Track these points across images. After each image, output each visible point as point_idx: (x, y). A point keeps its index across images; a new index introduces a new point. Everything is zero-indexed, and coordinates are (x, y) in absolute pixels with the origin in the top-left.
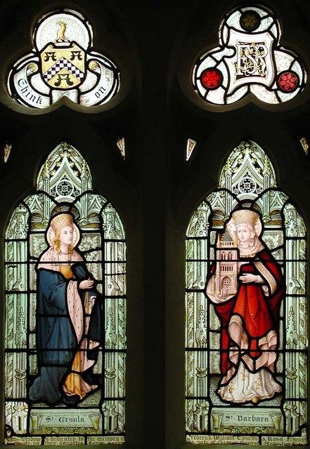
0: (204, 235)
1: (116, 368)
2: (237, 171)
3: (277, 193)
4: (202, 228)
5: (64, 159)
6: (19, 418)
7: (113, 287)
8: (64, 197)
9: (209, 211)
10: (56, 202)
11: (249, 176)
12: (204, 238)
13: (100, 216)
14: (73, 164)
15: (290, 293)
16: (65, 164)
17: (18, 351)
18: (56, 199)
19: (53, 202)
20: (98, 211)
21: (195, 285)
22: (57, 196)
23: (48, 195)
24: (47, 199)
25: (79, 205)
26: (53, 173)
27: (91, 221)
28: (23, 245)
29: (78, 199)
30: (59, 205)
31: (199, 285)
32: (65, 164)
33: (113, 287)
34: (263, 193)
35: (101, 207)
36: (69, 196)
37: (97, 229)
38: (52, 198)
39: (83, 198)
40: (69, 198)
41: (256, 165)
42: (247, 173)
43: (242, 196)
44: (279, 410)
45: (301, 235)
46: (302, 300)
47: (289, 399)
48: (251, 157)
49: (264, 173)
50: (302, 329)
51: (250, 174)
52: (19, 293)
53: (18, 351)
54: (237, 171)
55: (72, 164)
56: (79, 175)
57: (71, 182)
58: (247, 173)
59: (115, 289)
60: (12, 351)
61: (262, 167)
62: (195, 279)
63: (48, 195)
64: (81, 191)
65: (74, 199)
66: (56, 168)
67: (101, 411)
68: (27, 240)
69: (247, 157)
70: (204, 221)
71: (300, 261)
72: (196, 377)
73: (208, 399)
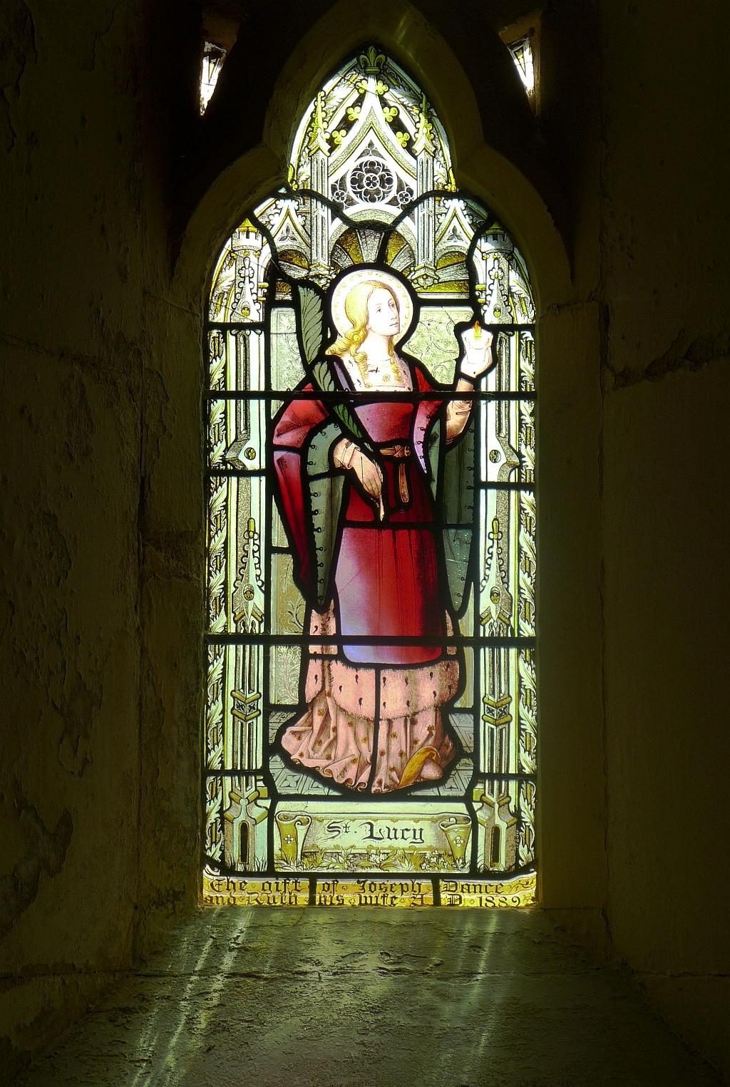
0: (255, 316)
1: (513, 693)
2: (344, 140)
3: (457, 205)
4: (248, 298)
5: (368, 95)
6: (244, 828)
7: (503, 459)
8: (370, 205)
9: (267, 249)
10: (346, 220)
11: (376, 153)
12: (253, 326)
13: (468, 263)
14: (393, 112)
15: (493, 477)
16: (371, 112)
17: (239, 639)
18: (349, 212)
19: (338, 221)
20: (465, 245)
21: (230, 456)
22: (351, 202)
23: (324, 201)
24: (323, 212)
25: (409, 228)
26: (339, 136)
27: (444, 276)
28: (256, 340)
29: (408, 210)
30: (356, 229)
31: (242, 457)
32: (371, 112)
33: (503, 459)
34: (414, 204)
35: (472, 234)
36: (380, 205)
37: (464, 297)
38: (336, 211)
39: (419, 211)
40: (384, 211)
41: (397, 125)
42: (371, 145)
43: (359, 210)
44: (461, 807)
45: (521, 320)
46: (528, 498)
47: (491, 776)
48: (384, 103)
49: (418, 147)
50: (527, 581)
51: (378, 146)
52: (245, 473)
53: (239, 639)
54: (344, 140)
55: (389, 114)
56: (409, 146)
57: (390, 164)
58: (371, 145)
59: (508, 463)
60: (225, 639)
61: (411, 129)
62: (232, 437)
63: (324, 201)
64: (417, 189)
65: (397, 211)
66: (347, 124)
67: (470, 808)
68: (264, 327)
69: (371, 101)
70: (254, 280)
71: (519, 396)
72: (230, 717)
73: (265, 773)
